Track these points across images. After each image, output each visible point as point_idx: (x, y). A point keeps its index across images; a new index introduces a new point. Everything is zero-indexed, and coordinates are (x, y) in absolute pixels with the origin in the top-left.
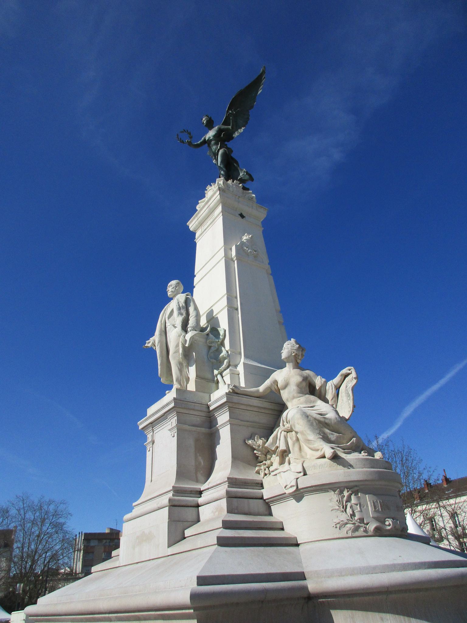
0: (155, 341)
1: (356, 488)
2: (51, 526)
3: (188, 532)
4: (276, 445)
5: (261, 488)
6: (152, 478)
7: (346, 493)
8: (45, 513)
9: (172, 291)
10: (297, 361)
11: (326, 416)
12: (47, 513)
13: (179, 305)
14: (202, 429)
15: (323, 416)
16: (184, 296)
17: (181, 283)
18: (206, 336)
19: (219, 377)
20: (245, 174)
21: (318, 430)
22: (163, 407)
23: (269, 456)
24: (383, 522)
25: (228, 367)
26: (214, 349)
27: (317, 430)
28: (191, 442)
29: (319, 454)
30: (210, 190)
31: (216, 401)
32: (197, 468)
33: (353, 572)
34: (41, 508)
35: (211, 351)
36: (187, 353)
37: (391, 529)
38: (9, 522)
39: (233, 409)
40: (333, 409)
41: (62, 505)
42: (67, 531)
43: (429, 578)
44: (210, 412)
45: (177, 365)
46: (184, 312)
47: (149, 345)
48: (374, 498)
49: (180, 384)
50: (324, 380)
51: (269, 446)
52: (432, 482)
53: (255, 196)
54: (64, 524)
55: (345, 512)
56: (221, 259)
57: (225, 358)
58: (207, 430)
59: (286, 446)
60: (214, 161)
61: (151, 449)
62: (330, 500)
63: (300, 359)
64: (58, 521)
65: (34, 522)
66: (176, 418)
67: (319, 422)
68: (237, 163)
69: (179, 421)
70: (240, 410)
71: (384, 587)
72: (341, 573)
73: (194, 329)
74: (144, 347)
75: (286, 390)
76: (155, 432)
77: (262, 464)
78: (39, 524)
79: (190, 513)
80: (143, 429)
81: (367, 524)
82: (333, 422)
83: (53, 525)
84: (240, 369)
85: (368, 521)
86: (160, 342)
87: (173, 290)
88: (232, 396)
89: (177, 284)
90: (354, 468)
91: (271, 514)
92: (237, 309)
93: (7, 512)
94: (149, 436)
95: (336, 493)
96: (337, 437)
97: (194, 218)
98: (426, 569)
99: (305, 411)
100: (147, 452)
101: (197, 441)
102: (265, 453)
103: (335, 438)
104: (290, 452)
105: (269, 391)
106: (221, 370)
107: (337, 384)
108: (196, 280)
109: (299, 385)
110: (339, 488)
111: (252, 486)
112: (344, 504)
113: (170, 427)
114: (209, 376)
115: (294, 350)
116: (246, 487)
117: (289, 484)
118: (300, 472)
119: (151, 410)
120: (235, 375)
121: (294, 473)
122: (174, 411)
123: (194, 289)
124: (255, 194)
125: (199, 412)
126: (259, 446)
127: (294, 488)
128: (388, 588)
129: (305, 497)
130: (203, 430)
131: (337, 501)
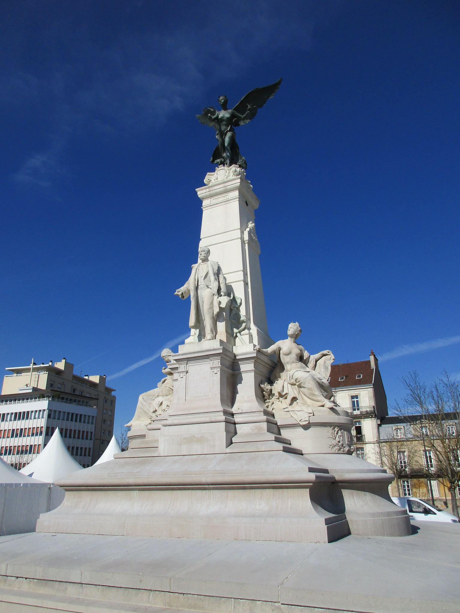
1: (341, 427)
9: (204, 256)
20: (244, 162)
23: (271, 397)
29: (321, 404)
62: (328, 432)
81: (344, 447)
82: (326, 385)
112: (335, 435)
129: (311, 428)
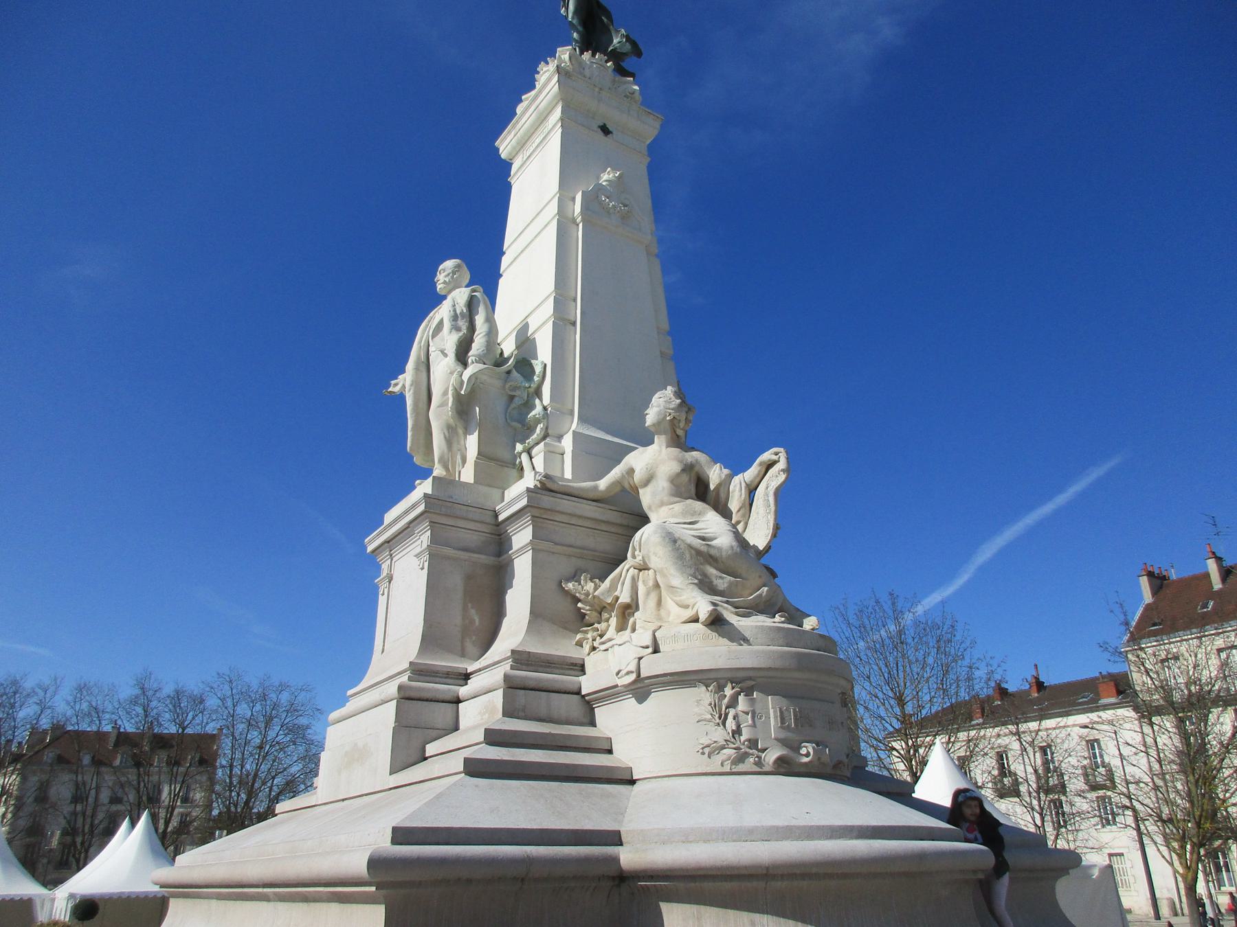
0: (405, 382)
2: (284, 730)
3: (431, 749)
4: (616, 594)
5: (582, 673)
6: (384, 646)
7: (728, 691)
8: (272, 707)
9: (445, 282)
10: (675, 432)
11: (713, 543)
12: (275, 706)
13: (455, 310)
14: (483, 557)
15: (704, 542)
16: (466, 292)
17: (465, 266)
18: (504, 375)
19: (524, 457)
20: (624, 40)
21: (693, 569)
22: (406, 512)
23: (605, 615)
24: (797, 749)
25: (544, 438)
26: (520, 403)
27: (691, 568)
28: (456, 581)
29: (689, 613)
30: (546, 72)
31: (510, 504)
32: (466, 631)
33: (708, 836)
34: (264, 697)
35: (513, 405)
36: (463, 406)
37: (810, 762)
38: (205, 721)
39: (541, 520)
40: (729, 530)
41: (303, 693)
42: (313, 740)
43: (827, 856)
44: (498, 525)
45: (442, 430)
46: (463, 324)
47: (397, 389)
48: (784, 702)
49: (447, 469)
50: (726, 471)
51: (603, 594)
52: (1012, 687)
53: (638, 89)
54: (308, 727)
55: (722, 727)
56: (552, 220)
57: (538, 421)
58: (492, 558)
59: (631, 596)
60: (563, 11)
61: (386, 590)
62: (698, 701)
63: (681, 427)
64: (296, 722)
65: (250, 724)
66: (429, 533)
67: (699, 553)
68: (609, 17)
69: (434, 539)
70: (556, 523)
71: (761, 867)
72: (687, 837)
73: (480, 360)
74: (386, 393)
75: (649, 489)
76: (394, 559)
77: (589, 628)
78: (262, 725)
79: (440, 713)
80: (374, 551)
81: (764, 750)
82: (724, 554)
83: (287, 729)
84: (567, 443)
85: (765, 746)
86: (415, 383)
87: (447, 280)
88: (539, 495)
89: (455, 267)
90: (751, 645)
91: (593, 723)
92: (574, 324)
93: (202, 701)
94: (385, 567)
95: (710, 689)
96: (731, 583)
97: (509, 132)
98: (851, 838)
99: (671, 530)
100: (380, 596)
101: (469, 578)
102: (599, 610)
103: (726, 585)
104: (637, 609)
105: (618, 489)
106: (528, 443)
107: (752, 482)
108: (505, 261)
109: (673, 480)
110: (716, 680)
111: (562, 669)
112: (723, 712)
113: (418, 550)
114: (506, 455)
115: (669, 409)
116: (548, 670)
117: (624, 668)
118: (647, 647)
119: (389, 517)
120: (554, 455)
121: (635, 647)
122: (424, 520)
123: (501, 281)
124: (639, 86)
125: (479, 525)
126: (587, 594)
127: (633, 677)
128: (767, 868)
130: (483, 559)
131: (710, 704)
